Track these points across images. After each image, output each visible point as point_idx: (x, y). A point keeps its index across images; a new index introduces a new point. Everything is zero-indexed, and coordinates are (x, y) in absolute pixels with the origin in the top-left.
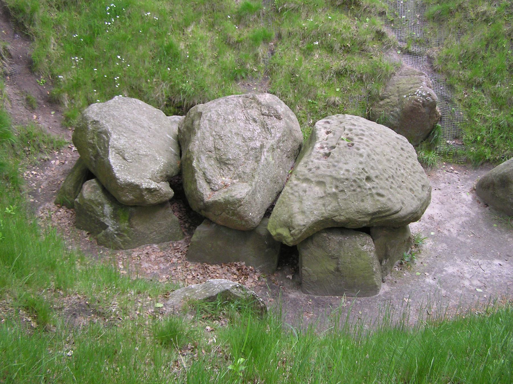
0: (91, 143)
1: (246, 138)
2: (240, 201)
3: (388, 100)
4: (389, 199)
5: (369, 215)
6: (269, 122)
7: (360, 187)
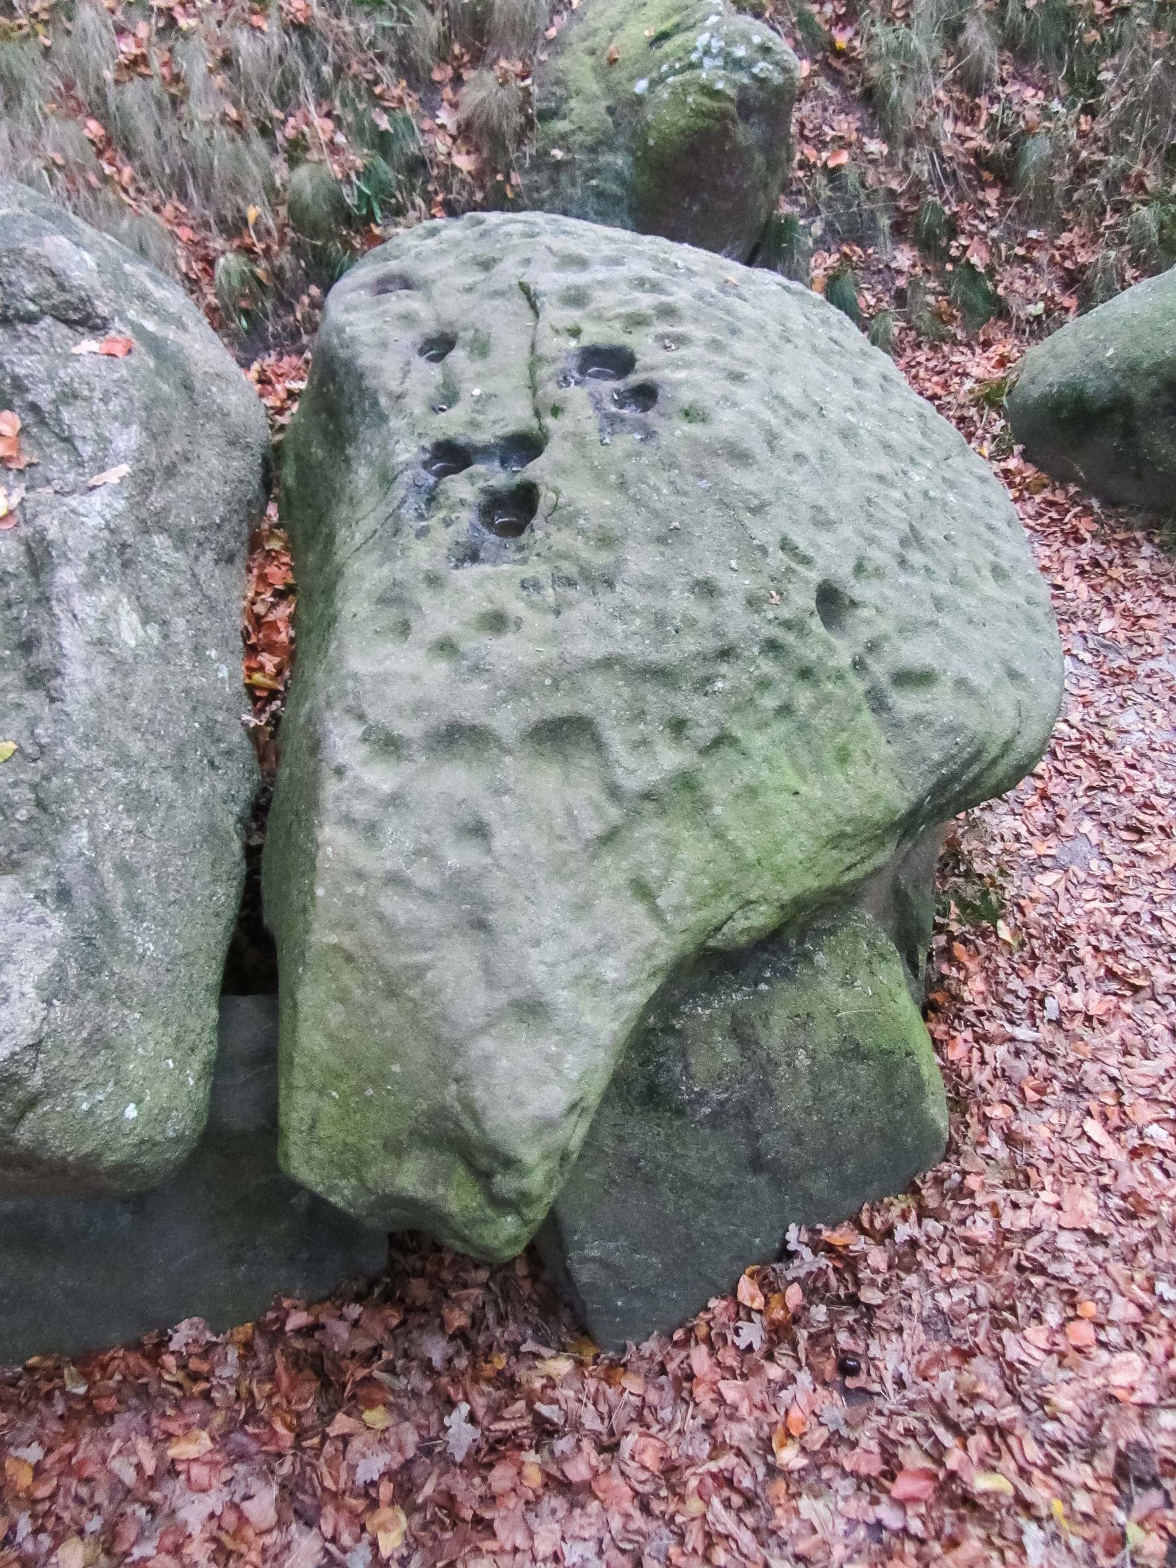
4: (961, 684)
7: (805, 674)
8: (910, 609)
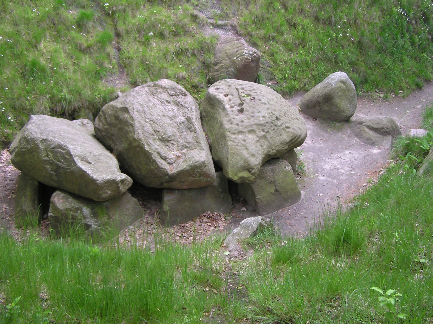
0: (47, 160)
1: (171, 116)
2: (204, 163)
3: (222, 64)
4: (293, 129)
5: (287, 143)
6: (180, 100)
7: (276, 126)
8: (286, 120)
